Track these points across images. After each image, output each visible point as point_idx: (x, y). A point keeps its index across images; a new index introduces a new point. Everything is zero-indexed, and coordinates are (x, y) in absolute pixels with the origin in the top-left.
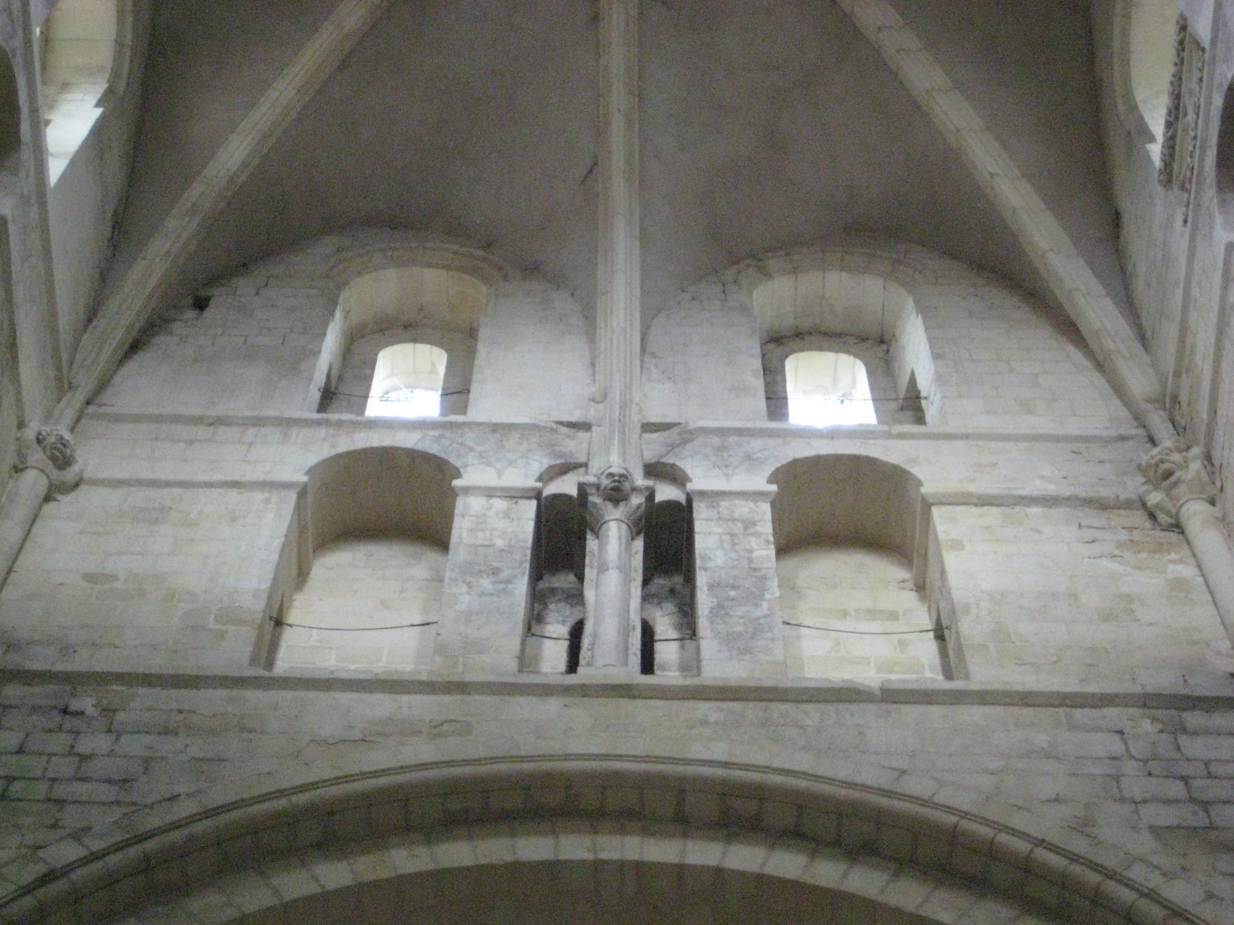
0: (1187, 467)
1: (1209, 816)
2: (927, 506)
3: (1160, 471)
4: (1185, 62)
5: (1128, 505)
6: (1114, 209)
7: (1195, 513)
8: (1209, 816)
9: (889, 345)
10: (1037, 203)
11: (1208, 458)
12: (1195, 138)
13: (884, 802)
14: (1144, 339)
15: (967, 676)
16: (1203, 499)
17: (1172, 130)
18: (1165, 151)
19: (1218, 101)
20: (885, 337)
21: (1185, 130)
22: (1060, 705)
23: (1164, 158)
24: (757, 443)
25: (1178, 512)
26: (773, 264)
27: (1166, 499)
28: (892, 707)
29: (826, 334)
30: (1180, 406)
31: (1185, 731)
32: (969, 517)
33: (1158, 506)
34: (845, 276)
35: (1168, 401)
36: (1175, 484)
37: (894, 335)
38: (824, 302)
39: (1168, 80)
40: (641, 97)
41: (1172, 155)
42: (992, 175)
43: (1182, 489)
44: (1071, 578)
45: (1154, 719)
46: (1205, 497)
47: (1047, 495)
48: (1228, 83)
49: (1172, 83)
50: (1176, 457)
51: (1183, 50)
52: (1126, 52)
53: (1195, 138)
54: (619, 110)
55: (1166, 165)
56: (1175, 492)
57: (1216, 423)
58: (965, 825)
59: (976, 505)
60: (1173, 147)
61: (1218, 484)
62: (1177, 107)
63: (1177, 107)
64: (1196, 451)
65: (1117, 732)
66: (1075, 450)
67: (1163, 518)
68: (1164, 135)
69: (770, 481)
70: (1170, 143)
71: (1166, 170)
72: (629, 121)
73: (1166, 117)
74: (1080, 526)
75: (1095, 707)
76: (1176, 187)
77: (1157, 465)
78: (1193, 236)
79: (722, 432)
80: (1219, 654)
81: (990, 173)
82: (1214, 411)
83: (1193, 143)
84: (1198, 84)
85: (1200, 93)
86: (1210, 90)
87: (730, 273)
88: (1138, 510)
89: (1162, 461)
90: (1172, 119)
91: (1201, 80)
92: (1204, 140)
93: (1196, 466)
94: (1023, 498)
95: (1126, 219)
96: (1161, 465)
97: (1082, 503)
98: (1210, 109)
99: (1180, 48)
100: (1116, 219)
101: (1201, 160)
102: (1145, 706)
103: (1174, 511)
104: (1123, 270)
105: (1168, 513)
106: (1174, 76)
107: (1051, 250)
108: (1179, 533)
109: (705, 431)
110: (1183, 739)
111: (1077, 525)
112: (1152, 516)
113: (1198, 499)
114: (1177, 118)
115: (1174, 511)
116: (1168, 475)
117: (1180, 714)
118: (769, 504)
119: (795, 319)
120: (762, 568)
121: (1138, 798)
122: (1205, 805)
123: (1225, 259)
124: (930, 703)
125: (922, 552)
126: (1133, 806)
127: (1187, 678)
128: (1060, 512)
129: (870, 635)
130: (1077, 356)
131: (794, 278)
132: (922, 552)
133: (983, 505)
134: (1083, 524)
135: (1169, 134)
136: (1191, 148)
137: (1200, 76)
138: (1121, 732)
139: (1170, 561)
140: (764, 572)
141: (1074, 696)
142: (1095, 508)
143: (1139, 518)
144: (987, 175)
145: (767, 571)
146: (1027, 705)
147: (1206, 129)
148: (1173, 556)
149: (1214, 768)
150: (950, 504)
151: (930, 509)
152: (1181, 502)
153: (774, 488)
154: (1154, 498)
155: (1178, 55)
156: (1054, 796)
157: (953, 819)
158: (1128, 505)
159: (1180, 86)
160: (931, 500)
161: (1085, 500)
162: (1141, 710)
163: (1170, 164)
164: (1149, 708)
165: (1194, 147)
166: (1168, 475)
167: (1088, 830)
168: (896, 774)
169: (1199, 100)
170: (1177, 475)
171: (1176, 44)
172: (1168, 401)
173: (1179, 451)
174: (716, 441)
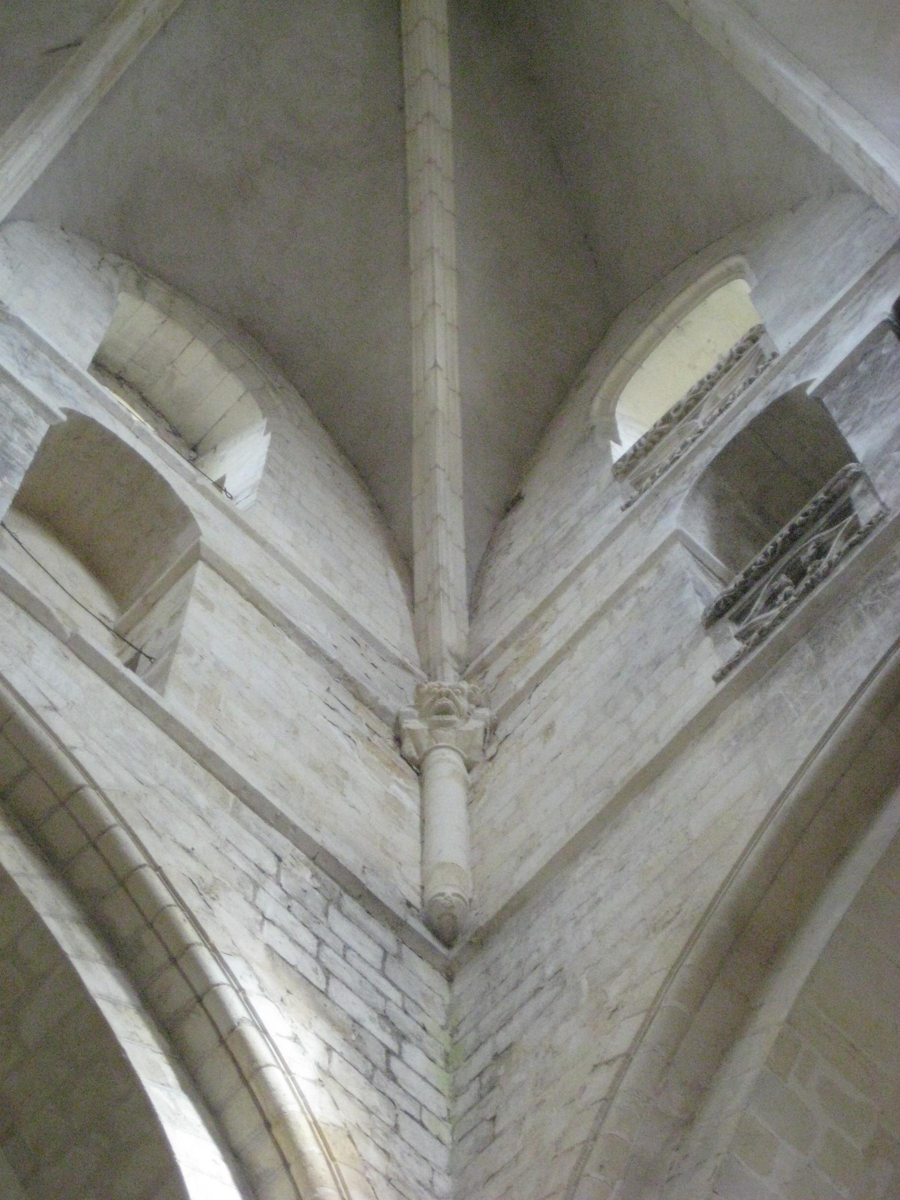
0: (467, 719)
1: (327, 984)
2: (196, 555)
3: (439, 702)
4: (730, 372)
5: (381, 713)
6: (517, 491)
7: (449, 761)
8: (327, 984)
9: (199, 456)
10: (456, 427)
11: (491, 729)
12: (701, 432)
13: (22, 712)
14: (474, 607)
15: (162, 693)
16: (463, 757)
17: (666, 426)
18: (644, 441)
19: (758, 405)
20: (200, 447)
21: (681, 433)
22: (233, 792)
23: (638, 446)
24: (63, 379)
25: (430, 751)
26: (158, 290)
27: (427, 733)
28: (72, 657)
29: (144, 399)
30: (484, 677)
31: (339, 908)
32: (227, 597)
33: (413, 733)
34: (211, 357)
35: (473, 666)
36: (442, 725)
37: (215, 448)
38: (169, 368)
39: (700, 378)
40: (164, 29)
41: (647, 450)
42: (436, 365)
43: (447, 735)
44: (299, 715)
45: (314, 875)
46: (466, 756)
47: (314, 642)
48: (787, 390)
49: (701, 383)
50: (464, 703)
51: (738, 358)
52: (636, 364)
53: (701, 432)
54: (145, 10)
55: (633, 456)
56: (440, 732)
57: (530, 698)
58: (91, 793)
59: (241, 594)
60: (654, 443)
61: (490, 752)
62: (688, 409)
63: (688, 409)
64: (485, 712)
65: (276, 855)
66: (356, 638)
67: (409, 747)
68: (655, 426)
69: (64, 410)
70: (655, 437)
71: (631, 459)
72: (142, 32)
73: (670, 410)
74: (328, 690)
75: (266, 820)
76: (627, 482)
77: (440, 695)
78: (627, 521)
79: (38, 342)
80: (406, 881)
81: (436, 362)
82: (535, 683)
83: (694, 436)
84: (745, 384)
85: (740, 393)
86: (755, 393)
87: (113, 258)
88: (387, 725)
89: (448, 695)
90: (674, 415)
91: (751, 381)
92: (710, 437)
93: (476, 724)
94: (290, 625)
95: (525, 505)
96: (444, 698)
97: (341, 676)
98: (741, 411)
99: (736, 355)
100: (513, 502)
101: (692, 457)
102: (313, 859)
103: (425, 748)
104: (490, 547)
105: (418, 750)
106: (709, 377)
107: (444, 470)
108: (415, 771)
109: (21, 326)
110: (333, 911)
111: (327, 687)
112: (398, 740)
113: (460, 753)
114: (680, 418)
115: (425, 748)
116: (445, 711)
117: (342, 893)
118: (48, 426)
119: (131, 360)
120: (14, 459)
121: (268, 915)
122: (328, 974)
123: (664, 542)
124: (112, 685)
125: (151, 600)
126: (260, 918)
127: (366, 870)
128: (316, 666)
129: (76, 599)
130: (396, 583)
131: (160, 321)
132: (151, 600)
133: (248, 600)
134: (332, 689)
135: (659, 428)
136: (689, 439)
137: (752, 376)
138: (279, 859)
139: (396, 781)
140: (13, 462)
141: (254, 793)
142: (351, 692)
143: (385, 731)
144: (430, 364)
145: (16, 464)
146: (202, 764)
147: (722, 427)
148: (401, 781)
149: (349, 954)
150: (219, 573)
151: (195, 562)
152: (440, 744)
153: (64, 417)
154: (413, 724)
155: (729, 360)
156: (190, 847)
157: (80, 779)
158: (381, 713)
159: (707, 390)
160: (203, 554)
161: (346, 675)
162: (307, 860)
163: (638, 458)
164: (315, 864)
165: (694, 440)
166: (445, 711)
167: (207, 897)
168: (47, 703)
169: (734, 399)
170: (453, 718)
171: (734, 349)
172: (473, 666)
173: (470, 700)
174: (28, 344)
